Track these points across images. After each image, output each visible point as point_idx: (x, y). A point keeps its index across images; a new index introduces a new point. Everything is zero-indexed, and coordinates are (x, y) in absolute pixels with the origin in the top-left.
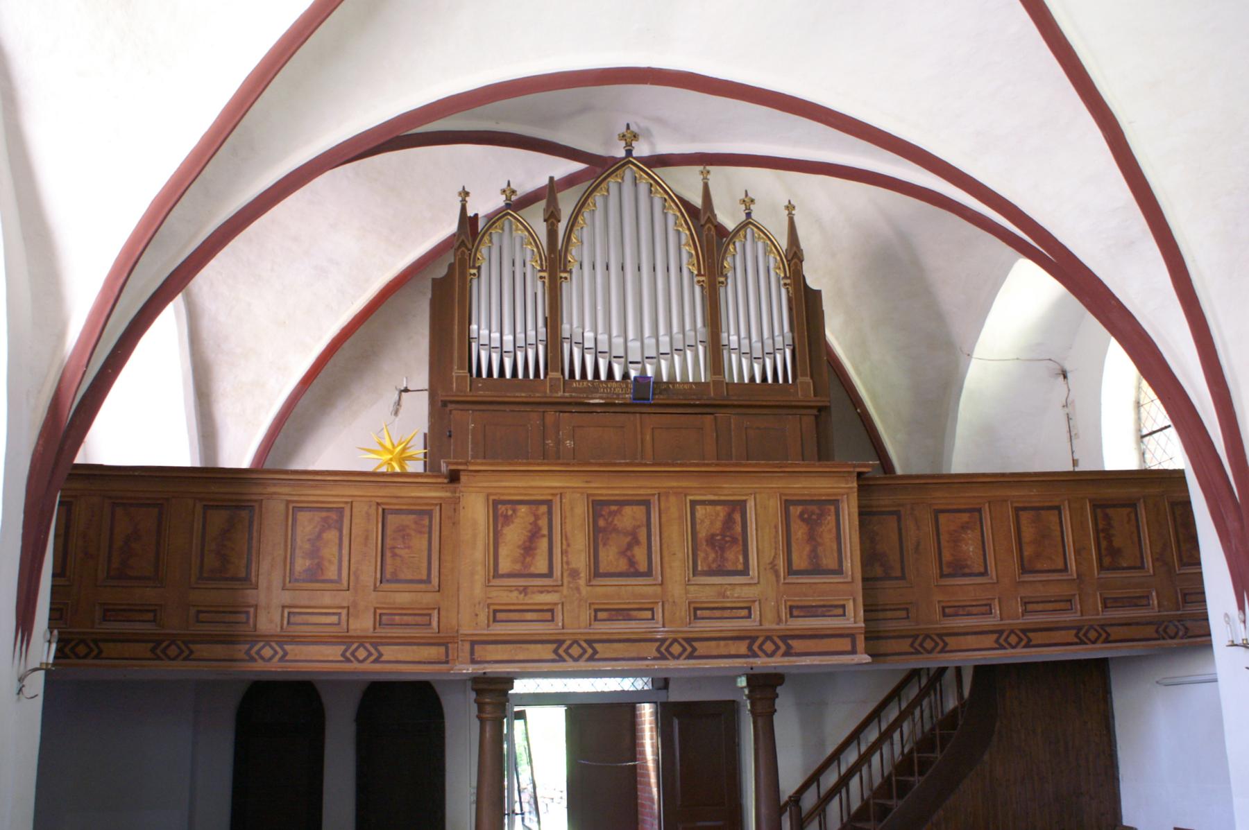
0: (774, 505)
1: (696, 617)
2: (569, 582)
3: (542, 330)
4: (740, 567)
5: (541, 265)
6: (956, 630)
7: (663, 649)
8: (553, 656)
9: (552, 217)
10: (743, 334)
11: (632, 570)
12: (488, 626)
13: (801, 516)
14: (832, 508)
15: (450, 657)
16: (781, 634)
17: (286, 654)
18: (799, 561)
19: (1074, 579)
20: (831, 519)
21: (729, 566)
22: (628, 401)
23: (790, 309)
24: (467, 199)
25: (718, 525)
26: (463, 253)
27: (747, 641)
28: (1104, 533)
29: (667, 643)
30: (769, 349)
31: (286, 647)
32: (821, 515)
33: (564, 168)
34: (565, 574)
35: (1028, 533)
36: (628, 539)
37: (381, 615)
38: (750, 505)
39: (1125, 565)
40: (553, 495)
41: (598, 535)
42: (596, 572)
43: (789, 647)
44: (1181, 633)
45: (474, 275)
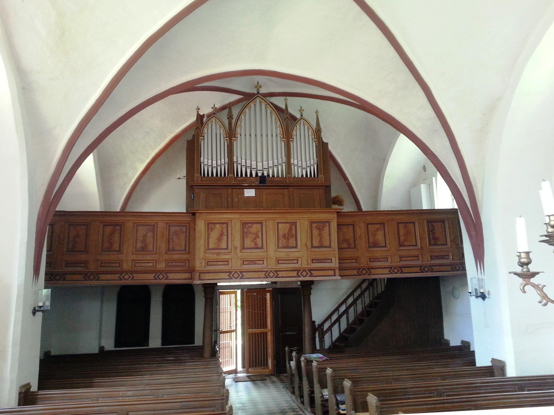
0: (306, 223)
1: (278, 263)
2: (234, 251)
3: (227, 159)
4: (294, 245)
5: (226, 135)
6: (374, 267)
7: (267, 274)
8: (228, 277)
9: (230, 117)
10: (299, 159)
11: (256, 247)
12: (205, 267)
13: (316, 227)
14: (328, 224)
15: (193, 277)
16: (308, 269)
17: (133, 277)
18: (315, 243)
19: (419, 249)
20: (327, 228)
21: (291, 245)
22: (257, 185)
23: (316, 149)
24: (199, 111)
25: (287, 230)
26: (198, 131)
27: (297, 272)
28: (432, 231)
29: (268, 272)
30: (308, 165)
31: (133, 275)
32: (323, 227)
33: (235, 97)
34: (233, 248)
35: (402, 232)
36: (254, 236)
37: (168, 262)
38: (298, 224)
39: (440, 244)
40: (228, 220)
41: (244, 235)
42: (243, 248)
43: (311, 274)
44: (461, 269)
45: (202, 139)
